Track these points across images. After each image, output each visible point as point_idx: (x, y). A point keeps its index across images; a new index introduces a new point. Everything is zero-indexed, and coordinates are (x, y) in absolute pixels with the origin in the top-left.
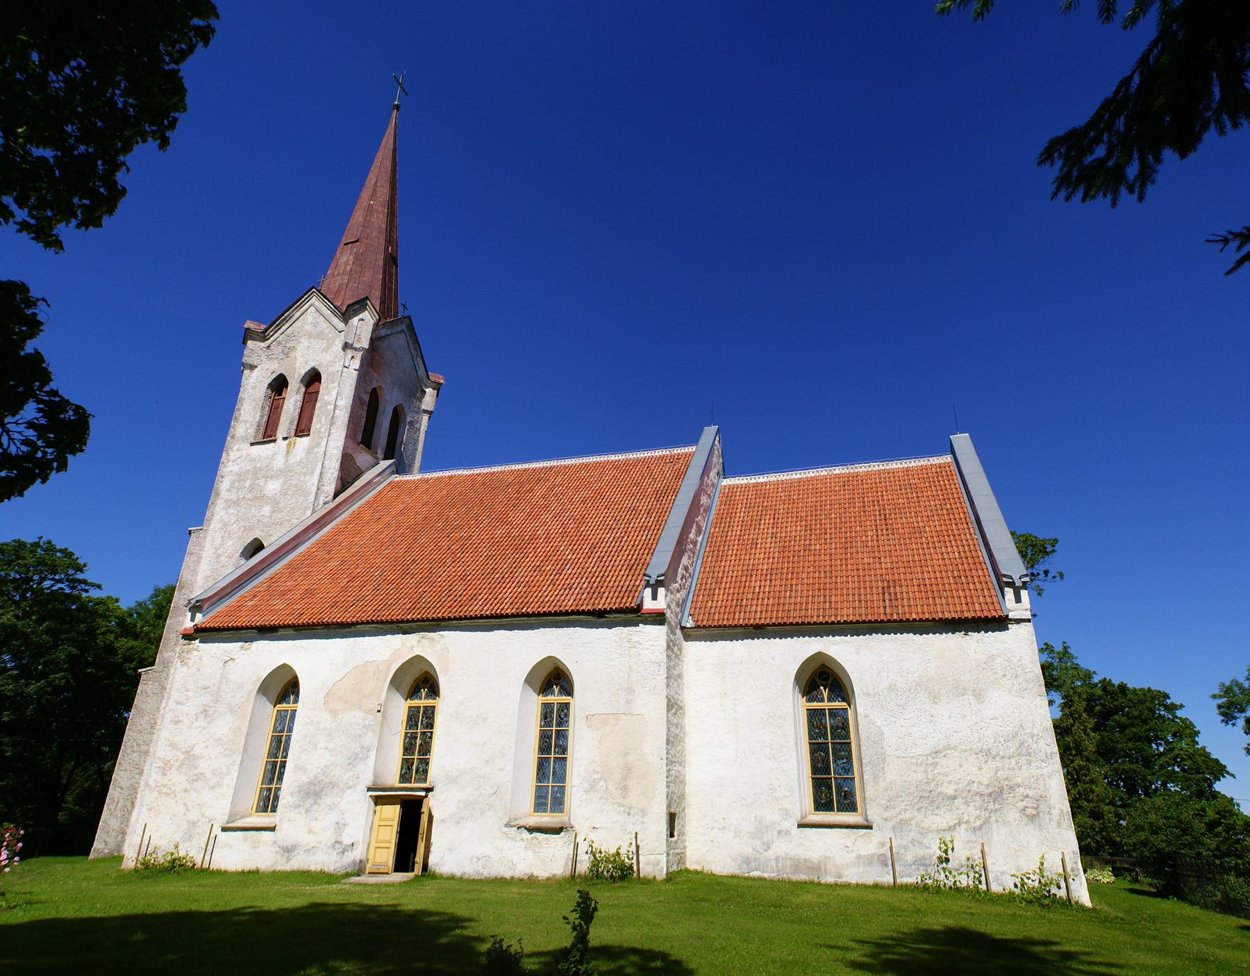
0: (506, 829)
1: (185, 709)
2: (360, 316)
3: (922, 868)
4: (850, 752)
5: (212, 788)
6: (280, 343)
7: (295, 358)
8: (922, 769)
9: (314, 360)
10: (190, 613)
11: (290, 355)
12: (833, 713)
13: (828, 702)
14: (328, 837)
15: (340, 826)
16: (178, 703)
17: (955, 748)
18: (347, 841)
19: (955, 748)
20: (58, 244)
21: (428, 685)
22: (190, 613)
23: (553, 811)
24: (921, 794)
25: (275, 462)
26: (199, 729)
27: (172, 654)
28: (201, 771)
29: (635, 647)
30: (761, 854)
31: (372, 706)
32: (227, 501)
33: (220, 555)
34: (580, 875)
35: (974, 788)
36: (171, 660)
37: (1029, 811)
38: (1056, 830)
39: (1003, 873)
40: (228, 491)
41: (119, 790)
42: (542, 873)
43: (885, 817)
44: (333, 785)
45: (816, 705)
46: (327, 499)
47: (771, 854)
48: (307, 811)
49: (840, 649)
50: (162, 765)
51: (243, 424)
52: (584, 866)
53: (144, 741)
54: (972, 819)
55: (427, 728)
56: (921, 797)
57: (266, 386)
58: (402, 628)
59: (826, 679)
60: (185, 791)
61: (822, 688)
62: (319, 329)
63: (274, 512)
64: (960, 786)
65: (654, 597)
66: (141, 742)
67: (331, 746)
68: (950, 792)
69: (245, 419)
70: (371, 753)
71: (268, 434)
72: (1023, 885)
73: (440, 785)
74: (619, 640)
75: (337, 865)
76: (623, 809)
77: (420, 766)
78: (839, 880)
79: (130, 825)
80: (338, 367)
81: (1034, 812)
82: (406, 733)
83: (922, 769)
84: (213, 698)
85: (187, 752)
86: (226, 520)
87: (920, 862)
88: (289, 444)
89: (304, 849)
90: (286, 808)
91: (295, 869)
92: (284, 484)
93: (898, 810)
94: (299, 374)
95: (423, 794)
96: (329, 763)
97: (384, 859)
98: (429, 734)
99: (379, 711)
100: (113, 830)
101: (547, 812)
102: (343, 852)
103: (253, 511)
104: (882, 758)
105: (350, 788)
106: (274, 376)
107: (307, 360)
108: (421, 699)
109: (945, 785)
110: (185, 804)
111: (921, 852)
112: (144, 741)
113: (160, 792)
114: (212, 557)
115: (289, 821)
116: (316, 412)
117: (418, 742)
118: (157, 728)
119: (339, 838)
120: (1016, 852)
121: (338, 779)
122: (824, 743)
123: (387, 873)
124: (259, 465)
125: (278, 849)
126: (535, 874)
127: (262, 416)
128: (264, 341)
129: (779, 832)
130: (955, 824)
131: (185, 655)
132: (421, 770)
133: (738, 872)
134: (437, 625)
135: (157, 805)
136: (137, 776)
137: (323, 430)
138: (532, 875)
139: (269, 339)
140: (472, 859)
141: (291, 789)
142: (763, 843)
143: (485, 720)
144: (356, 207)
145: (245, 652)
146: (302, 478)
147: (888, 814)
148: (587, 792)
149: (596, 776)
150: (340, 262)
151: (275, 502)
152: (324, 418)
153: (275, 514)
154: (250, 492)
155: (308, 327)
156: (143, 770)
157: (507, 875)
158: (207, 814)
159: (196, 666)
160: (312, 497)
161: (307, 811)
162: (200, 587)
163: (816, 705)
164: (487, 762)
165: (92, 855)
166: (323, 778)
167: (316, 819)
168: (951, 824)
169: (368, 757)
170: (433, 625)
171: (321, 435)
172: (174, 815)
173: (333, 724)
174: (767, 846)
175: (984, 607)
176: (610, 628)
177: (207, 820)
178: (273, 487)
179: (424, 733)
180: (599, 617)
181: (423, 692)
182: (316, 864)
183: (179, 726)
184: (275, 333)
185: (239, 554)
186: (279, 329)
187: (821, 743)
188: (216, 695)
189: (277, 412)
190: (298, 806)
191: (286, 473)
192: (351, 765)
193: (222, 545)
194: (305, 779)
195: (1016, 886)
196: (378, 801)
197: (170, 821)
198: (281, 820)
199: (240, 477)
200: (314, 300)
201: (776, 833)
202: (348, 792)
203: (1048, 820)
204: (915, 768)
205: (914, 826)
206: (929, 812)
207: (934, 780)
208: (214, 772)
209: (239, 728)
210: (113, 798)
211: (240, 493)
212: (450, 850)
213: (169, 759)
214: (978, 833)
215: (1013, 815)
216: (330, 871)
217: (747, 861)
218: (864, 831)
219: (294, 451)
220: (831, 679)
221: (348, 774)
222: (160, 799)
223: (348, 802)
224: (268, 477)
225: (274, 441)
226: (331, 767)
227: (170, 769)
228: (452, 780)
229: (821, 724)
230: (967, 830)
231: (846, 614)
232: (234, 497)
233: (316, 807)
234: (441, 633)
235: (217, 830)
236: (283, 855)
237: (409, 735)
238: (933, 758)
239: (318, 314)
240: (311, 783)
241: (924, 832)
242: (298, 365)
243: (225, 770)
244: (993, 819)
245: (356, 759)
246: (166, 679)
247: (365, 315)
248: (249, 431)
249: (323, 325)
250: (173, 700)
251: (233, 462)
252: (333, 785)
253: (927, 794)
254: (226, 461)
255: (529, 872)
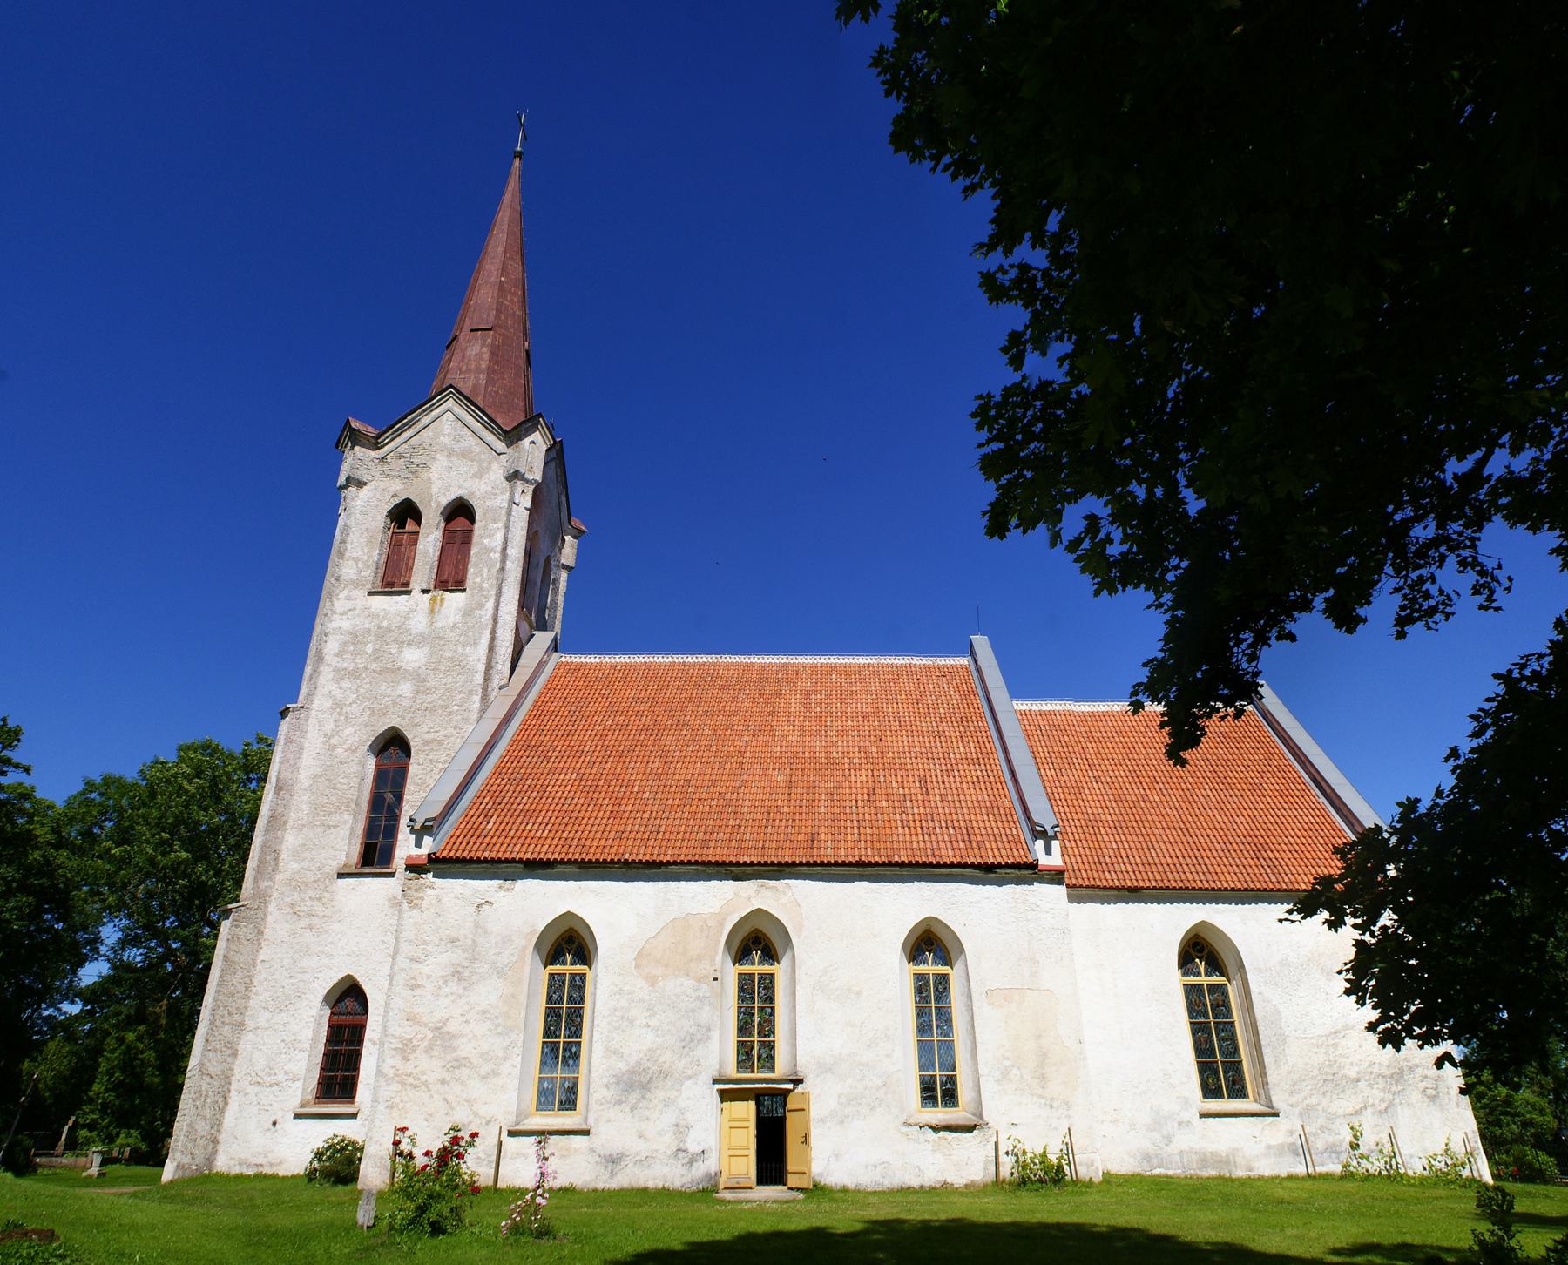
0: (905, 1129)
1: (425, 969)
2: (531, 438)
3: (1333, 1155)
4: (1233, 1033)
5: (484, 1078)
6: (401, 456)
7: (429, 479)
8: (1323, 1050)
9: (460, 487)
10: (414, 836)
11: (419, 474)
12: (1213, 988)
13: (1206, 975)
14: (667, 1143)
15: (681, 1129)
16: (412, 960)
17: (1353, 1027)
18: (694, 1148)
19: (1353, 1027)
20: (1145, 665)
21: (761, 946)
22: (414, 836)
23: (945, 1105)
24: (1325, 1077)
25: (412, 622)
26: (453, 998)
27: (270, 883)
28: (464, 1055)
29: (1032, 910)
30: (1161, 1149)
31: (705, 972)
32: (337, 670)
33: (334, 747)
34: (1004, 1180)
35: (1376, 1069)
36: (269, 891)
37: (1429, 1092)
38: (1456, 1110)
39: (1412, 1156)
40: (336, 655)
41: (208, 1079)
42: (958, 1179)
43: (1290, 1102)
44: (664, 1074)
45: (1192, 980)
46: (502, 683)
47: (1173, 1148)
48: (633, 1109)
49: (1227, 919)
50: (400, 1046)
51: (351, 562)
52: (1007, 1167)
53: (237, 1009)
54: (1377, 1102)
55: (765, 1002)
56: (1325, 1081)
57: (385, 513)
58: (731, 872)
59: (1201, 950)
60: (443, 1082)
61: (1197, 960)
62: (463, 445)
63: (418, 692)
64: (1362, 1068)
65: (1048, 851)
66: (233, 1010)
67: (654, 1022)
68: (1353, 1074)
69: (354, 555)
70: (712, 1033)
71: (393, 580)
72: (1430, 1167)
73: (811, 1076)
74: (1011, 900)
75: (684, 1180)
76: (1043, 1101)
77: (762, 1050)
78: (1251, 1174)
79: (223, 1130)
80: (502, 500)
81: (1434, 1093)
82: (739, 1008)
83: (1323, 1050)
84: (466, 955)
85: (437, 1029)
86: (339, 697)
87: (1332, 1150)
88: (433, 600)
89: (634, 1160)
90: (602, 1104)
91: (625, 1186)
92: (431, 654)
93: (1303, 1095)
94: (438, 503)
95: (790, 1086)
96: (654, 1046)
97: (743, 1170)
98: (769, 1010)
99: (715, 979)
100: (201, 1138)
101: (937, 1106)
102: (691, 1163)
103: (383, 688)
104: (1283, 1039)
105: (689, 1078)
106: (397, 500)
107: (450, 486)
108: (753, 964)
109: (1347, 1067)
110: (445, 1100)
111: (1331, 1139)
112: (237, 1009)
113: (403, 1084)
114: (321, 749)
115: (609, 1121)
116: (473, 559)
117: (756, 1019)
118: (254, 990)
119: (682, 1145)
120: (1421, 1133)
121: (671, 1067)
122: (1205, 1023)
123: (750, 1188)
124: (385, 624)
125: (597, 1159)
126: (949, 1181)
127: (380, 555)
128: (375, 450)
129: (1180, 1124)
130: (1361, 1109)
131: (412, 892)
132: (764, 1056)
133: (1138, 1170)
134: (780, 871)
135: (402, 1101)
136: (229, 1060)
137: (486, 585)
138: (945, 1183)
139: (382, 447)
140: (867, 1167)
141: (605, 1080)
142: (1164, 1137)
143: (859, 993)
144: (479, 282)
145: (506, 893)
146: (460, 649)
147: (1293, 1100)
148: (999, 1082)
149: (1008, 1063)
150: (468, 354)
151: (418, 679)
152: (485, 570)
153: (420, 696)
154: (375, 660)
155: (446, 440)
156: (237, 1050)
157: (915, 1183)
158: (481, 1113)
159: (433, 910)
160: (479, 678)
161: (633, 1109)
162: (305, 790)
163: (1192, 980)
164: (869, 1046)
165: (169, 1172)
166: (649, 1064)
167: (648, 1119)
168: (1357, 1108)
169: (708, 1038)
170: (773, 871)
171: (485, 593)
172: (431, 1115)
173: (652, 994)
174: (1169, 1140)
175: (957, 852)
176: (1000, 885)
177: (484, 1122)
178: (413, 657)
179: (751, 1035)
180: (988, 872)
181: (757, 955)
182: (655, 1179)
183: (418, 992)
184: (393, 440)
185: (367, 747)
186: (398, 436)
187: (1202, 1023)
188: (471, 951)
189: (399, 552)
190: (620, 1102)
191: (432, 639)
192: (686, 1049)
193: (336, 732)
194: (622, 1066)
195: (1425, 1169)
196: (725, 1096)
197: (426, 1123)
198: (597, 1120)
199: (355, 639)
200: (450, 403)
201: (1176, 1125)
202: (688, 1083)
203: (1447, 1100)
204: (1315, 1050)
205: (1321, 1111)
206: (1335, 1096)
207: (1336, 1062)
208: (484, 1056)
209: (513, 996)
210: (200, 1091)
211: (357, 661)
212: (836, 1156)
213: (409, 1037)
214: (1384, 1116)
215: (1415, 1096)
216: (676, 1187)
217: (1147, 1157)
218: (1271, 1118)
219: (442, 610)
220: (1206, 951)
221: (684, 1061)
222: (404, 1092)
223: (689, 1099)
224: (402, 642)
225: (409, 592)
226: (658, 1051)
227: (414, 1051)
228: (826, 1069)
229: (1200, 1001)
230: (1373, 1113)
231: (1230, 881)
232: (348, 664)
233: (644, 1103)
234: (786, 881)
235: (504, 1133)
236: (606, 1167)
237: (743, 1010)
238: (1333, 1039)
239: (460, 424)
240: (632, 1072)
241: (1331, 1118)
242: (434, 490)
243: (500, 1054)
244: (1397, 1101)
245: (692, 1041)
246: (262, 919)
247: (536, 436)
248: (363, 574)
249: (472, 441)
250: (404, 955)
251: (341, 614)
252: (664, 1074)
253: (1330, 1077)
254: (329, 612)
255: (941, 1178)
